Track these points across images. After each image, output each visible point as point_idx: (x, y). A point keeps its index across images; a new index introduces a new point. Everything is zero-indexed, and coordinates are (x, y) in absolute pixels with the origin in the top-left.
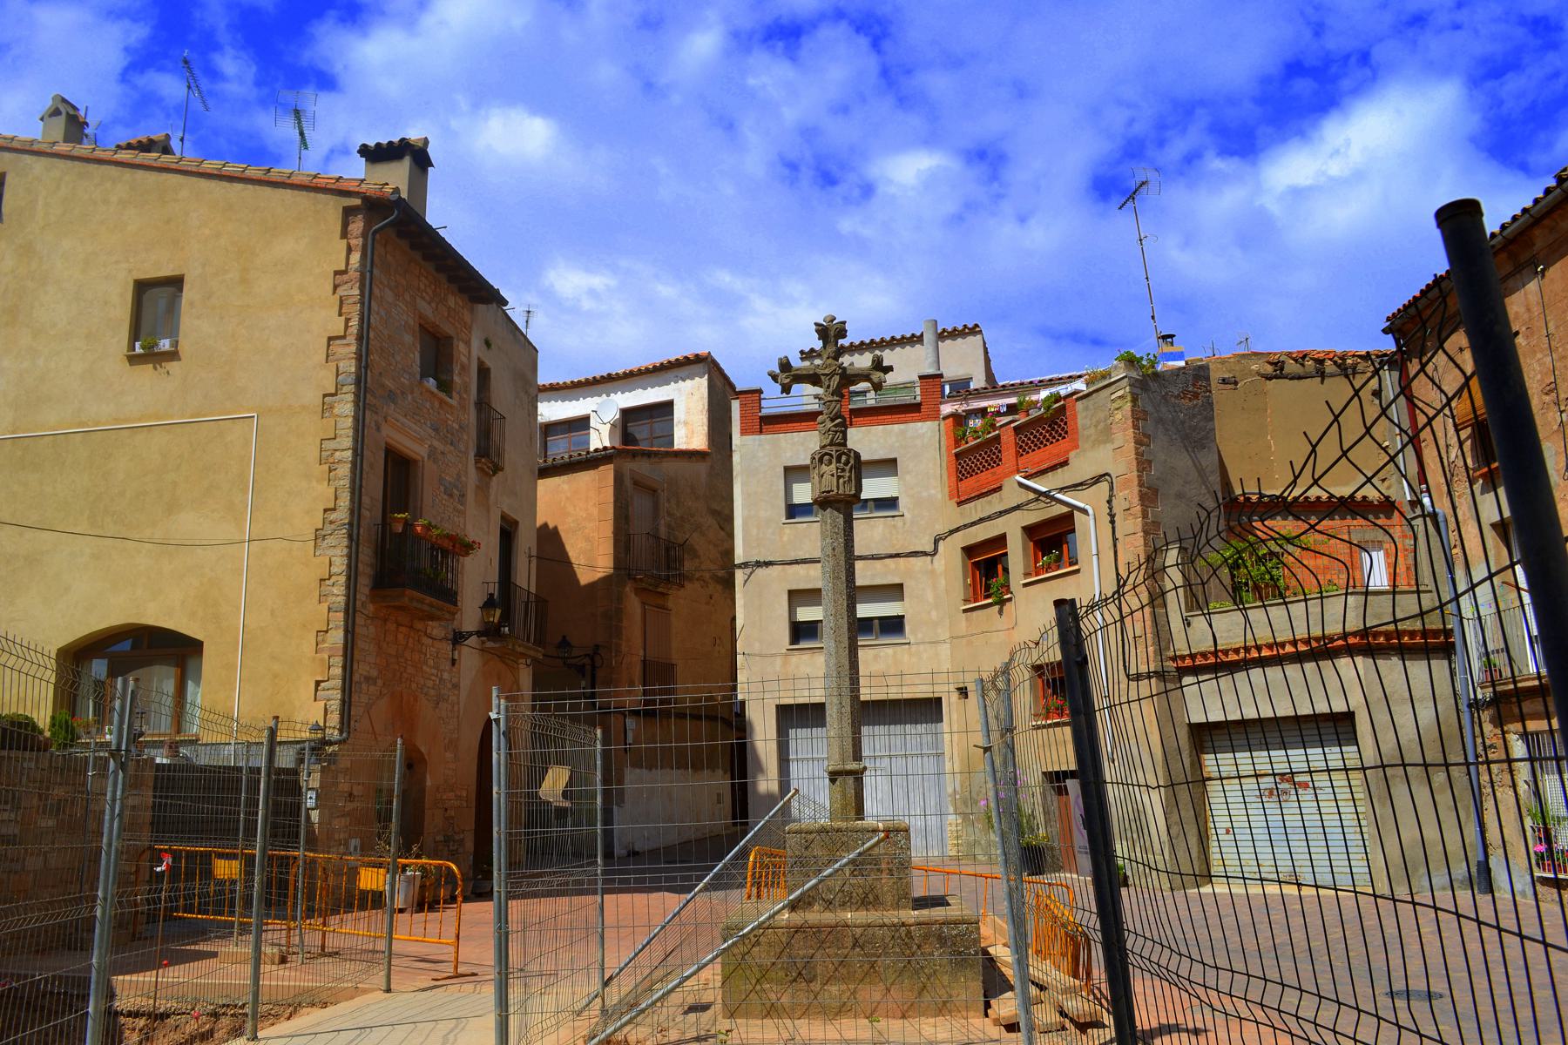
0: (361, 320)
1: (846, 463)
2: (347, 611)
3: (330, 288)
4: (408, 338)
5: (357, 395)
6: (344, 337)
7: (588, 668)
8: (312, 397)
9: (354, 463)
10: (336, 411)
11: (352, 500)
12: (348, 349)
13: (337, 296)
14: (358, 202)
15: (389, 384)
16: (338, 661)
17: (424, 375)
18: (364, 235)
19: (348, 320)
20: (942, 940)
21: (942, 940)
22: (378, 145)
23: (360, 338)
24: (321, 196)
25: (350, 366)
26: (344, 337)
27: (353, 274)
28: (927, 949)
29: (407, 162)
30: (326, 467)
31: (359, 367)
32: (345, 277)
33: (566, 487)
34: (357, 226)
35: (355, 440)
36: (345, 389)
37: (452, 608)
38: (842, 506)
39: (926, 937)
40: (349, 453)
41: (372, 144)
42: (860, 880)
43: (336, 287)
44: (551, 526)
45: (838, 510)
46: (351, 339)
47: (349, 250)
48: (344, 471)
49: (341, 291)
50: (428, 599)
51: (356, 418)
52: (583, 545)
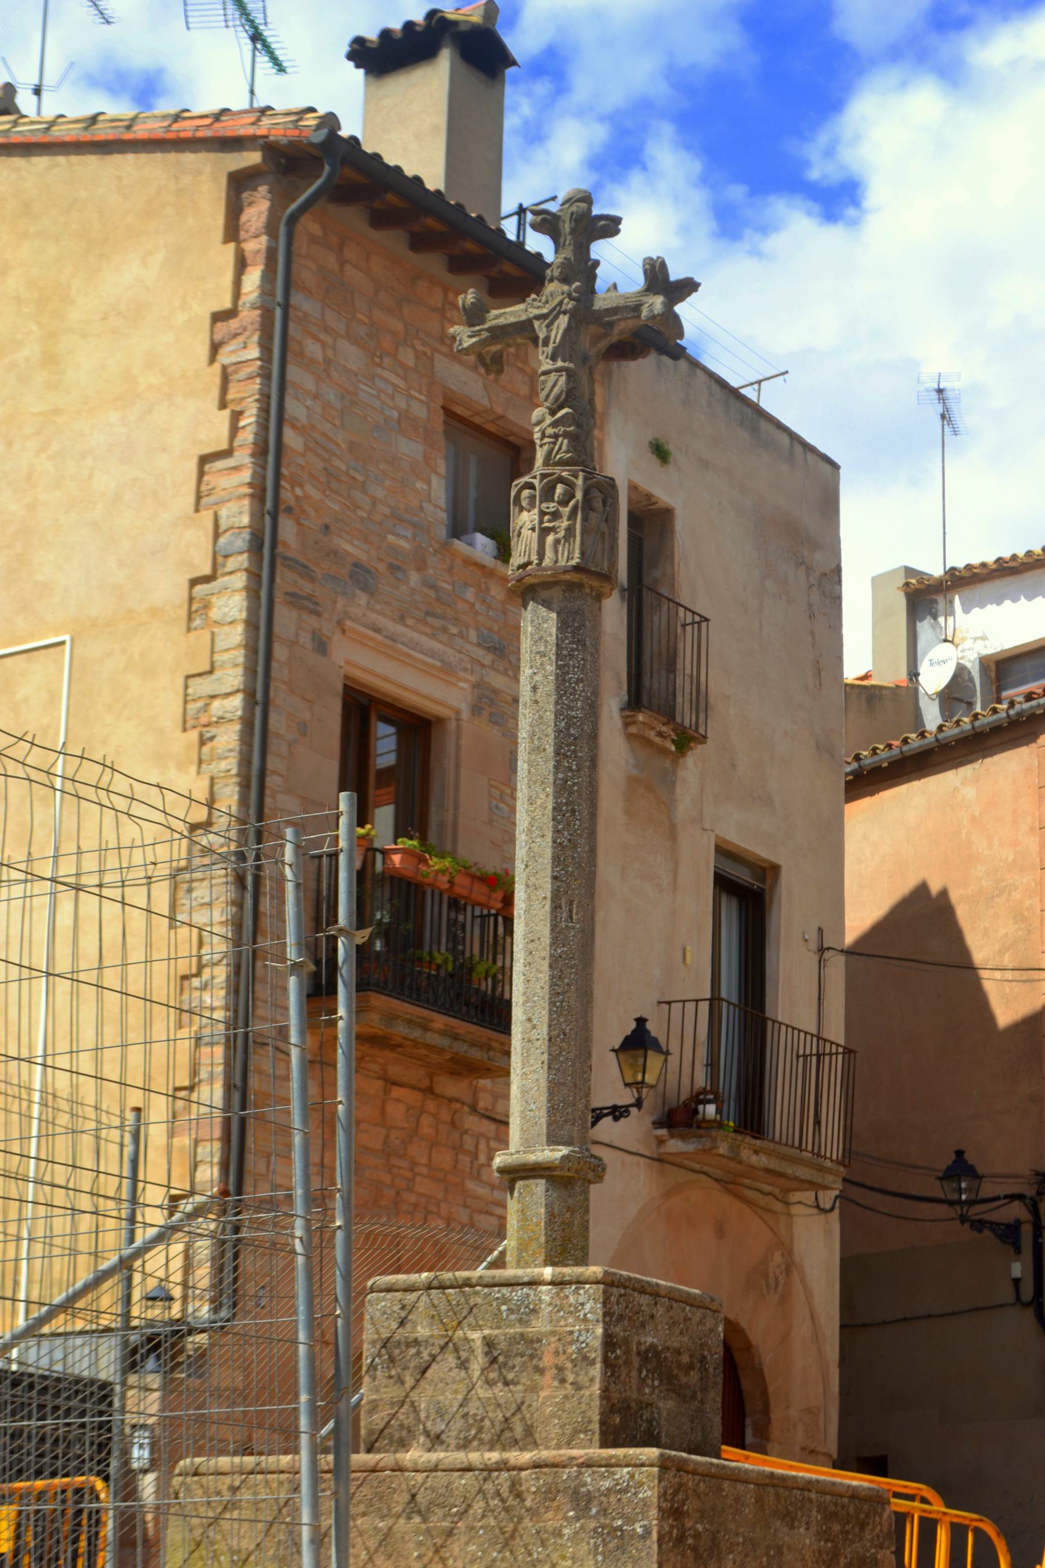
0: (264, 410)
1: (569, 496)
2: (230, 1043)
3: (204, 350)
4: (410, 449)
5: (254, 575)
6: (227, 453)
7: (1027, 1230)
8: (168, 588)
9: (247, 723)
10: (214, 614)
11: (243, 801)
12: (235, 479)
13: (217, 367)
14: (253, 158)
15: (352, 548)
16: (211, 1152)
17: (457, 530)
18: (271, 229)
19: (236, 416)
20: (582, 1500)
21: (582, 1500)
22: (386, 34)
23: (260, 451)
24: (189, 158)
25: (238, 514)
26: (227, 453)
27: (249, 316)
28: (551, 1520)
29: (445, 61)
30: (193, 735)
31: (257, 516)
32: (234, 324)
33: (969, 792)
34: (257, 211)
35: (250, 670)
36: (232, 564)
37: (501, 1037)
38: (556, 594)
39: (549, 1494)
40: (236, 702)
41: (372, 34)
42: (500, 1392)
43: (215, 348)
44: (935, 888)
45: (547, 604)
46: (243, 456)
47: (241, 264)
48: (228, 738)
49: (225, 357)
50: (440, 1021)
51: (251, 624)
52: (1007, 929)
